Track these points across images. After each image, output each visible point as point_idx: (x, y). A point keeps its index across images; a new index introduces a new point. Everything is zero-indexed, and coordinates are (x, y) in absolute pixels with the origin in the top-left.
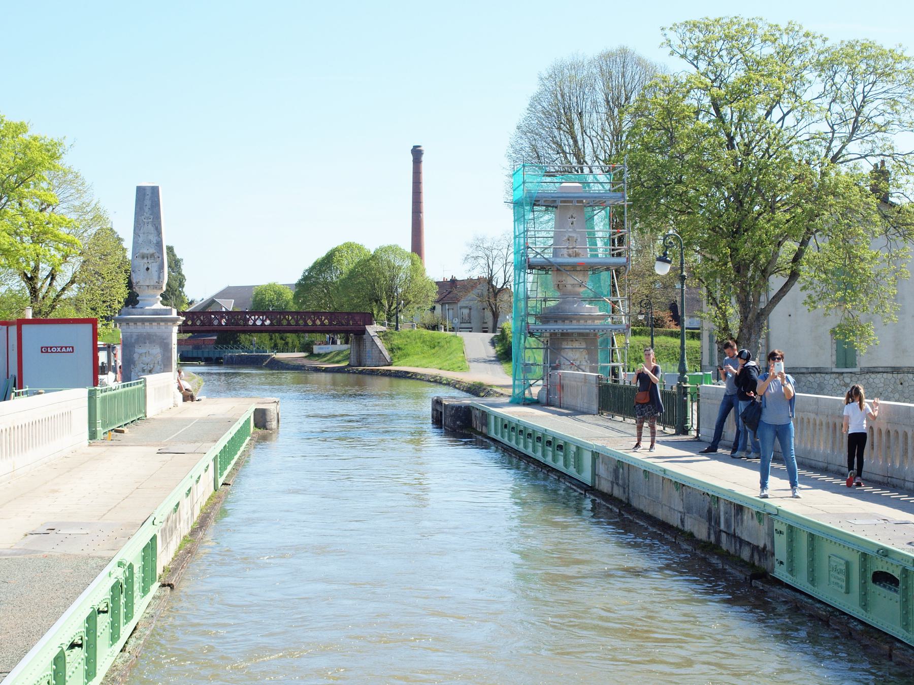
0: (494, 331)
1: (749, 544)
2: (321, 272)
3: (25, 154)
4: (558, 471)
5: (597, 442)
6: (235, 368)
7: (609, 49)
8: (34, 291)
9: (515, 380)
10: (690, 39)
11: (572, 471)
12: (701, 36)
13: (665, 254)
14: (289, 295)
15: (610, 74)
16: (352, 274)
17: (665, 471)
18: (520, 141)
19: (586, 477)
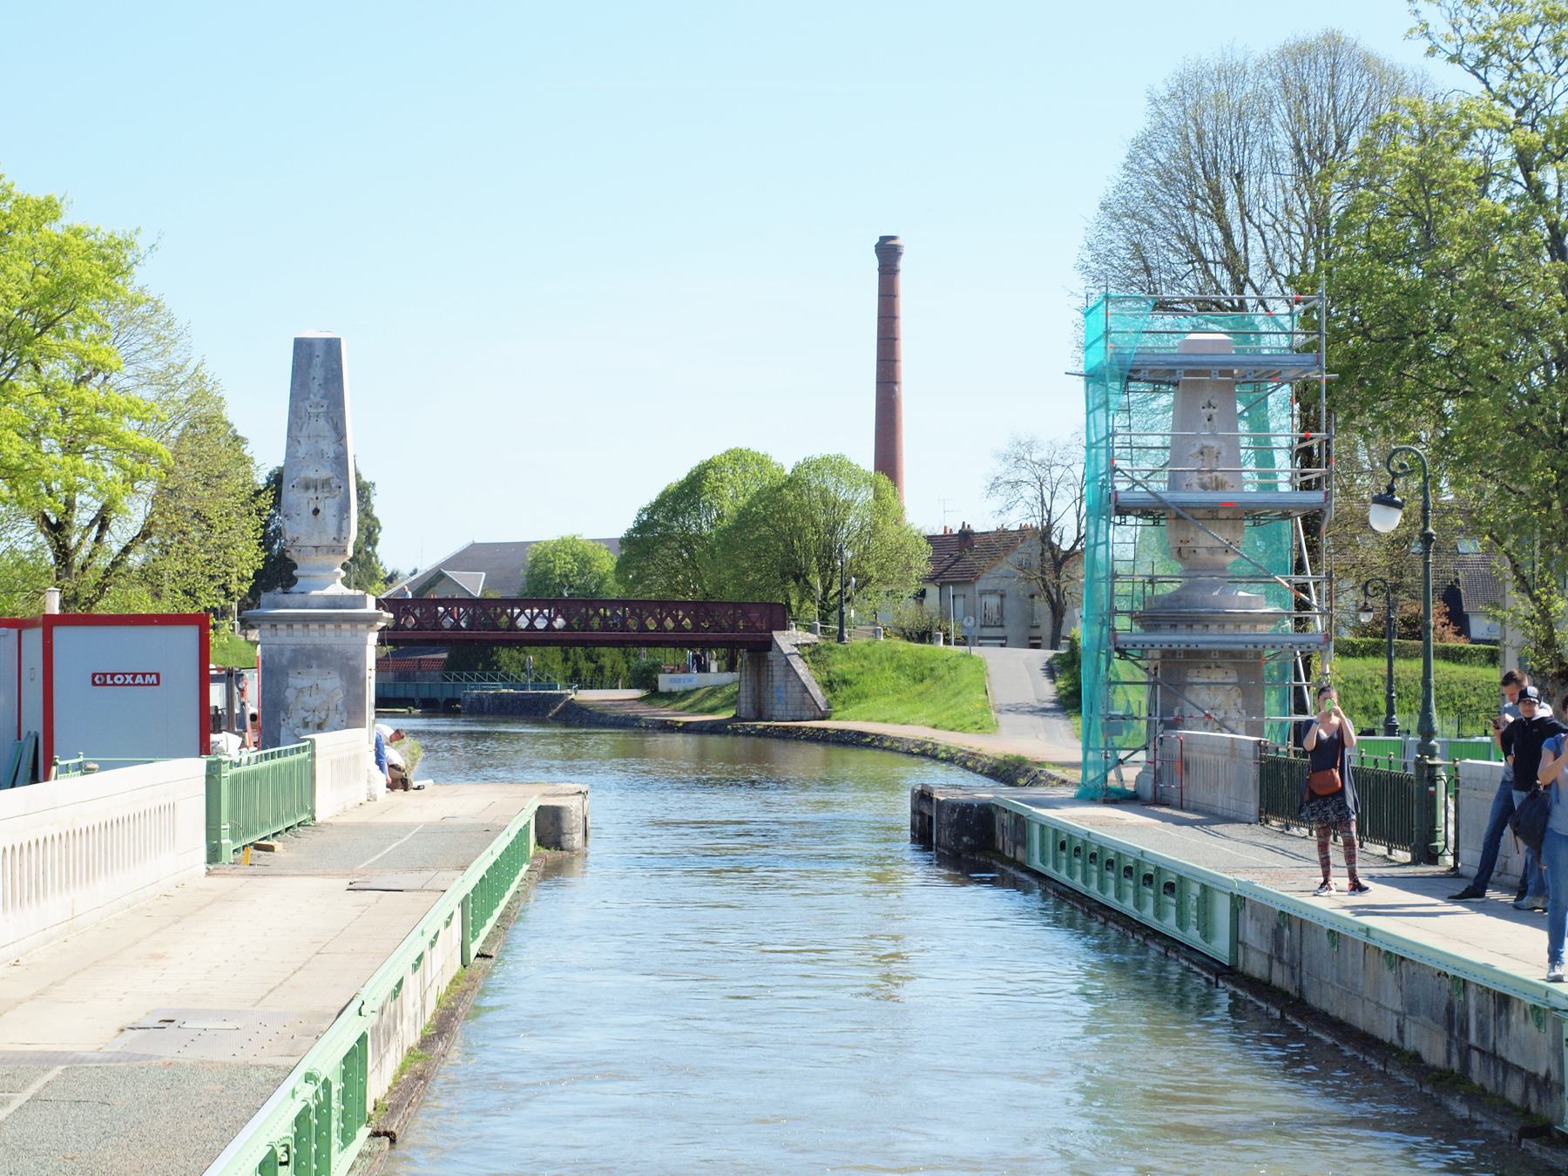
0: (1054, 646)
1: (1520, 1070)
2: (675, 513)
3: (54, 265)
4: (1165, 937)
5: (1238, 878)
6: (487, 723)
7: (1301, 36)
8: (63, 554)
9: (1086, 749)
10: (1471, 21)
11: (1192, 936)
12: (1494, 15)
13: (1391, 489)
14: (607, 563)
15: (1304, 90)
16: (745, 519)
17: (1368, 930)
18: (1107, 236)
19: (1220, 947)
